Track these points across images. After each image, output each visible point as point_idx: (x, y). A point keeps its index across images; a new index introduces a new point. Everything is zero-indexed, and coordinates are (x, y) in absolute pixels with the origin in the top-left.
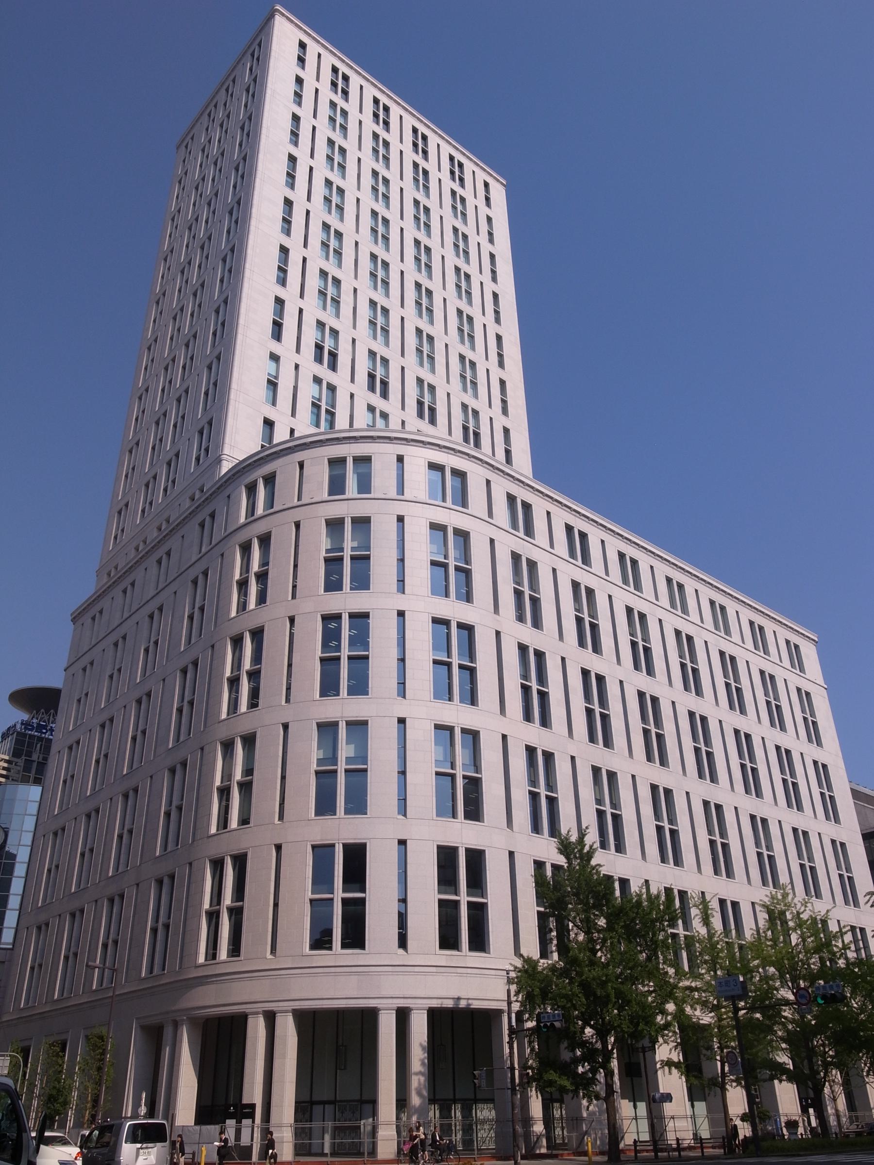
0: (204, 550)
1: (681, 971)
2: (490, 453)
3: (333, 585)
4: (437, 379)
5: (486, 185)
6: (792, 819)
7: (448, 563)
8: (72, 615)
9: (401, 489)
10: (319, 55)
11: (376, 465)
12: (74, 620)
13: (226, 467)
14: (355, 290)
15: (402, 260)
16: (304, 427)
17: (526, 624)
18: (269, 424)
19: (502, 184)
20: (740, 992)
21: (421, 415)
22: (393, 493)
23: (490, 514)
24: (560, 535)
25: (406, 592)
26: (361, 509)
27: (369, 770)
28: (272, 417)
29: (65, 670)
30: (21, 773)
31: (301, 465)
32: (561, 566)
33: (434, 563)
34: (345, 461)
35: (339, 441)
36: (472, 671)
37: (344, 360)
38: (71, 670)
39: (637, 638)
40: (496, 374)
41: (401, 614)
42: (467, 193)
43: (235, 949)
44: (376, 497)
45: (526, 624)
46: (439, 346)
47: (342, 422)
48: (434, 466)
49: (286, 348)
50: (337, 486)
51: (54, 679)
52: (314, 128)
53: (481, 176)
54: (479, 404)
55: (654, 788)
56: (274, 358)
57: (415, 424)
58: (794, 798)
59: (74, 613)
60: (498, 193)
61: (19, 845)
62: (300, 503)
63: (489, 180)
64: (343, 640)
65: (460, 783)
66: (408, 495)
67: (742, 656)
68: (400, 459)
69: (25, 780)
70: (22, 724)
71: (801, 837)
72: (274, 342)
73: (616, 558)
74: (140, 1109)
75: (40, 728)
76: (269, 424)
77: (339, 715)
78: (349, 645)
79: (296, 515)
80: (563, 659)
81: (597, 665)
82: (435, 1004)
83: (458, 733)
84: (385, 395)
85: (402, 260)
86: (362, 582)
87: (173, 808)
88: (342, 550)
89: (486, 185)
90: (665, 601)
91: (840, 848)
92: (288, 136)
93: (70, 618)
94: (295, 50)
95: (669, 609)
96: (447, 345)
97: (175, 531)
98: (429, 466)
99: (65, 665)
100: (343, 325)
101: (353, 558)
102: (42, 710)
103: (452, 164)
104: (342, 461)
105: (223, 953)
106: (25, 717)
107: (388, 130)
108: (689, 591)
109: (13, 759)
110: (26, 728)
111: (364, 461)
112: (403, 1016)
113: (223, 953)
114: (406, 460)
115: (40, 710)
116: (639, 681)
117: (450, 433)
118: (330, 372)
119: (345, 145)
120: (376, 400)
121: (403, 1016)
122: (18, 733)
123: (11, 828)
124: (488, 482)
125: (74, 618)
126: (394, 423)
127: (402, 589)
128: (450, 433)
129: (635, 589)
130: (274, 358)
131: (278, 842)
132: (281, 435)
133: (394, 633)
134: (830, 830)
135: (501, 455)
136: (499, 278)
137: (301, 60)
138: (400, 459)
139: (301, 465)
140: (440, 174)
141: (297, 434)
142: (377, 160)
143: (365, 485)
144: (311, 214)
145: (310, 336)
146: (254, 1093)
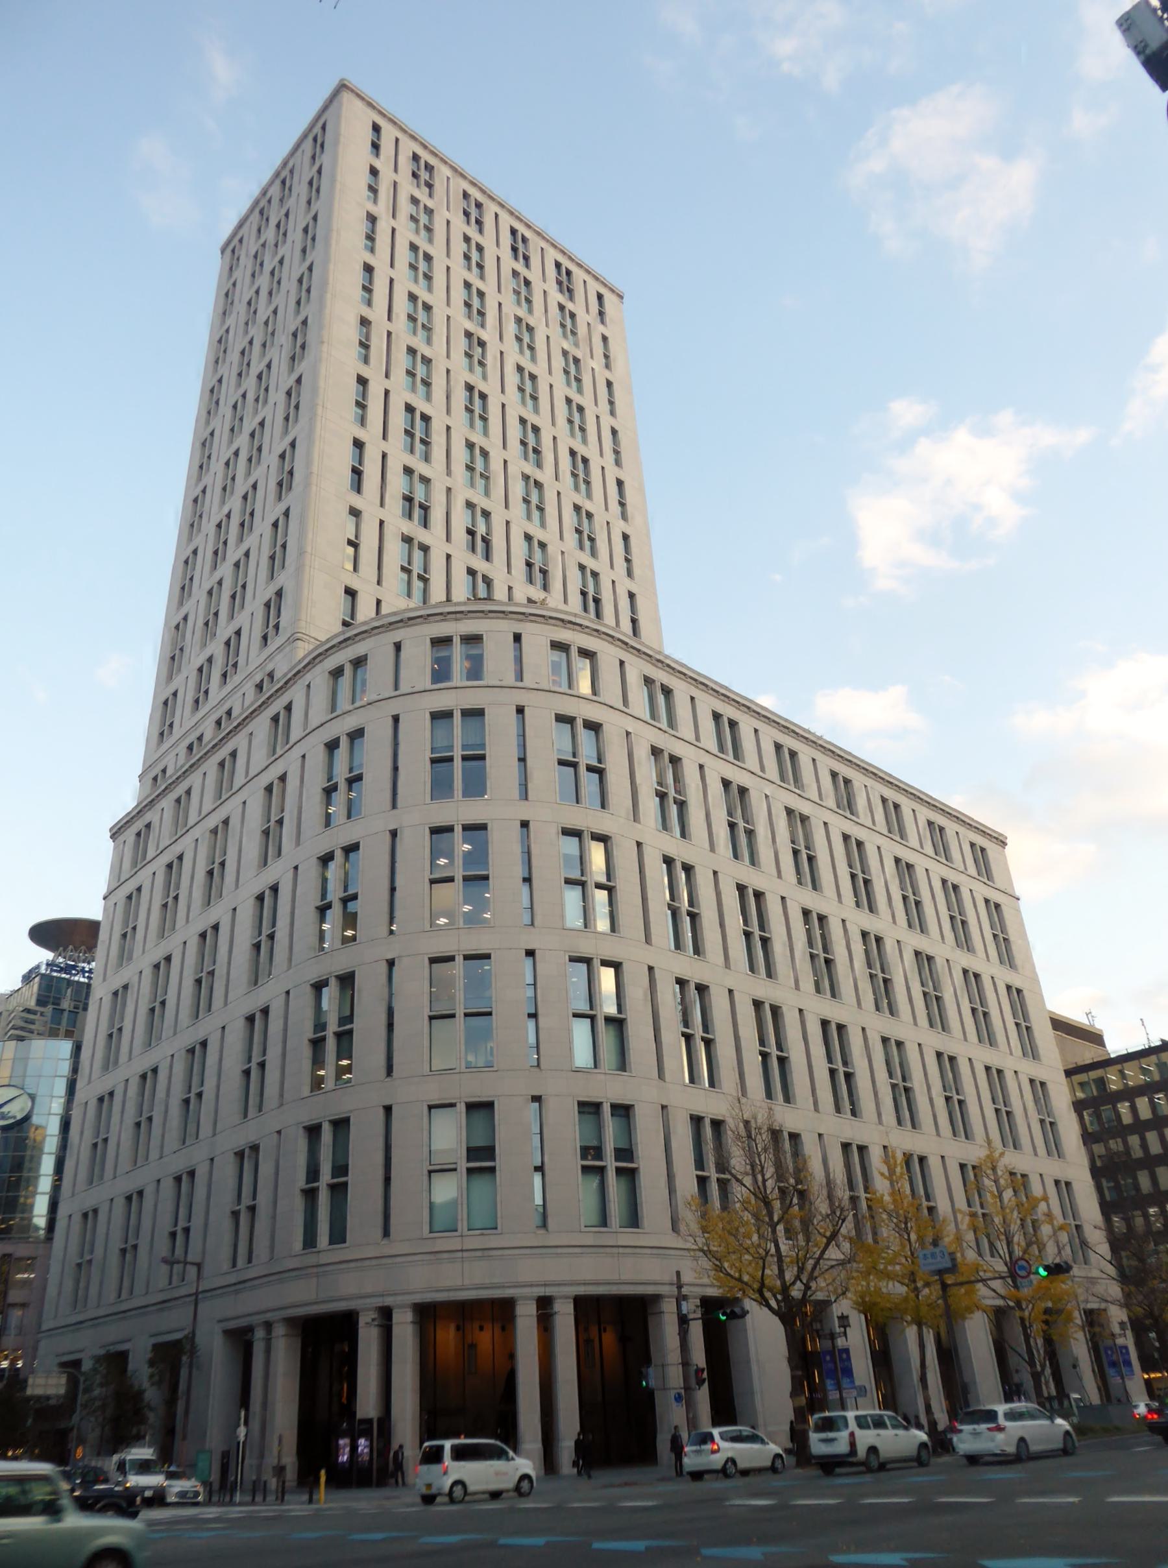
0: (279, 752)
1: (31, 1188)
2: (613, 624)
3: (441, 788)
5: (600, 297)
6: (985, 1056)
7: (578, 763)
8: (111, 830)
9: (520, 676)
10: (397, 140)
11: (489, 645)
12: (114, 836)
14: (448, 428)
15: (503, 391)
16: (396, 602)
17: (743, 861)
20: (949, 1265)
22: (510, 680)
23: (625, 702)
25: (530, 797)
26: (471, 700)
28: (355, 585)
29: (105, 898)
30: (49, 1026)
31: (398, 647)
33: (562, 763)
34: (452, 640)
35: (444, 616)
37: (437, 515)
38: (113, 899)
39: (799, 846)
40: (619, 526)
43: (338, 1235)
44: (491, 683)
45: (743, 861)
46: (437, 426)
47: (437, 593)
48: (557, 646)
49: (367, 501)
50: (441, 674)
51: (91, 908)
52: (393, 230)
55: (825, 1023)
56: (355, 513)
57: (523, 591)
58: (937, 1017)
61: (50, 1114)
62: (397, 693)
64: (456, 858)
66: (528, 681)
67: (817, 816)
68: (517, 638)
69: (53, 1034)
70: (48, 965)
71: (996, 1075)
73: (772, 749)
74: (239, 1430)
75: (67, 969)
77: (455, 947)
78: (464, 864)
79: (394, 707)
81: (755, 880)
82: (582, 1290)
85: (503, 391)
86: (476, 787)
87: (254, 1065)
88: (451, 748)
89: (600, 297)
90: (772, 772)
91: (1039, 1087)
93: (109, 834)
94: (369, 135)
96: (559, 493)
97: (241, 727)
98: (552, 646)
99: (104, 890)
100: (434, 470)
101: (465, 758)
102: (71, 947)
103: (559, 273)
104: (446, 641)
105: (323, 1239)
107: (481, 231)
108: (804, 760)
109: (38, 1008)
110: (52, 970)
111: (473, 639)
112: (544, 1304)
113: (323, 1239)
114: (524, 639)
115: (68, 947)
117: (566, 601)
118: (421, 530)
119: (482, 287)
120: (412, 528)
121: (544, 1304)
122: (43, 975)
123: (39, 1094)
124: (622, 663)
125: (114, 834)
126: (500, 593)
127: (525, 796)
128: (566, 601)
130: (355, 513)
131: (387, 1103)
132: (365, 611)
133: (517, 849)
134: (1028, 1068)
135: (626, 626)
136: (618, 411)
137: (376, 146)
138: (517, 638)
139: (398, 647)
141: (385, 610)
142: (469, 269)
143: (475, 671)
145: (397, 484)
146: (367, 1406)
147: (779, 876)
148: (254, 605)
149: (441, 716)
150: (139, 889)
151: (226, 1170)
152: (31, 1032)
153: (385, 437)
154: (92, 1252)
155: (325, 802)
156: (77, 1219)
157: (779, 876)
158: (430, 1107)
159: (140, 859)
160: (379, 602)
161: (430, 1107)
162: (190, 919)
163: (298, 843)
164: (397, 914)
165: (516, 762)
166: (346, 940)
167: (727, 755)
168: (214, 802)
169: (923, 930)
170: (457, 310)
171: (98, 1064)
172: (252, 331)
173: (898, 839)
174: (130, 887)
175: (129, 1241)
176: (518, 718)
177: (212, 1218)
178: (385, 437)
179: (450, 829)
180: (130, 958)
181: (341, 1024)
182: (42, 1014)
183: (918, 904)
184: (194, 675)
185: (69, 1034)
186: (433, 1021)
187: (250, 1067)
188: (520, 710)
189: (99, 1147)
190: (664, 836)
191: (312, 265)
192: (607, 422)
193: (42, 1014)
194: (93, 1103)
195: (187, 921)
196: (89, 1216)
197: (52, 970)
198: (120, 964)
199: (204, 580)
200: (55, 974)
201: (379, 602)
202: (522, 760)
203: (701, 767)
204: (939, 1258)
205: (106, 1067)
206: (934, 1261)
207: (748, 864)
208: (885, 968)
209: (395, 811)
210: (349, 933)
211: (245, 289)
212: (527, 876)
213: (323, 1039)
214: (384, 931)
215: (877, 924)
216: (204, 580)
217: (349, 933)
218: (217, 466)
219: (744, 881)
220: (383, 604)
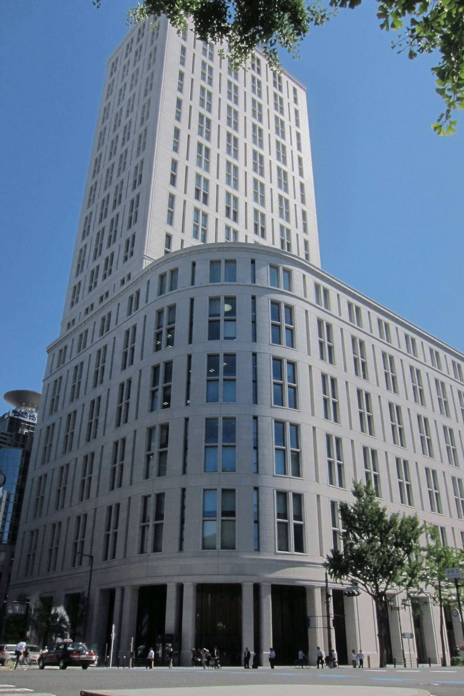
4: (266, 210)
5: (295, 90)
8: (47, 348)
12: (48, 351)
13: (146, 263)
18: (169, 238)
19: (304, 89)
21: (256, 232)
24: (345, 309)
26: (230, 292)
27: (237, 446)
29: (43, 381)
32: (345, 327)
34: (220, 262)
36: (295, 389)
38: (47, 382)
41: (254, 355)
42: (284, 95)
50: (214, 277)
53: (292, 84)
54: (291, 226)
59: (48, 347)
60: (302, 95)
63: (296, 87)
65: (289, 455)
66: (258, 284)
69: (16, 446)
72: (172, 187)
76: (169, 238)
80: (347, 383)
81: (365, 386)
83: (288, 425)
84: (205, 201)
89: (295, 90)
92: (179, 60)
93: (46, 350)
95: (348, 322)
99: (43, 378)
106: (14, 407)
109: (10, 433)
110: (15, 415)
111: (231, 262)
112: (180, 588)
114: (256, 262)
116: (389, 396)
118: (204, 205)
129: (358, 325)
140: (288, 100)
144: (193, 108)
147: (378, 385)
148: (121, 241)
149: (214, 300)
150: (61, 378)
151: (102, 516)
152: (4, 443)
153: (187, 159)
154: (35, 549)
155: (155, 338)
156: (28, 534)
157: (378, 385)
158: (205, 490)
159: (61, 361)
160: (182, 241)
161: (205, 490)
162: (87, 393)
163: (142, 358)
164: (191, 395)
165: (253, 523)
166: (164, 407)
167: (355, 324)
168: (99, 337)
169: (448, 415)
170: (224, 95)
171: (31, 513)
172: (122, 104)
173: (437, 369)
174: (56, 376)
175: (54, 545)
176: (252, 266)
177: (95, 537)
178: (187, 159)
179: (218, 299)
180: (56, 410)
181: (169, 324)
182: (10, 436)
183: (446, 402)
184: (89, 275)
185: (23, 446)
186: (210, 383)
187: (122, 405)
188: (253, 262)
189: (39, 501)
190: (321, 362)
191: (147, 128)
192: (294, 129)
193: (10, 436)
194: (36, 479)
195: (85, 394)
196: (43, 479)
197: (15, 415)
198: (51, 413)
199: (95, 230)
200: (16, 417)
201: (182, 241)
202: (257, 522)
203: (342, 330)
204: (455, 573)
205: (43, 462)
206: (452, 574)
207: (362, 378)
208: (437, 487)
209: (191, 345)
210: (166, 403)
211: (111, 133)
212: (256, 519)
213: (161, 333)
214: (184, 403)
215: (425, 412)
216: (95, 230)
217: (166, 403)
218: (103, 171)
219: (361, 387)
220: (185, 242)
